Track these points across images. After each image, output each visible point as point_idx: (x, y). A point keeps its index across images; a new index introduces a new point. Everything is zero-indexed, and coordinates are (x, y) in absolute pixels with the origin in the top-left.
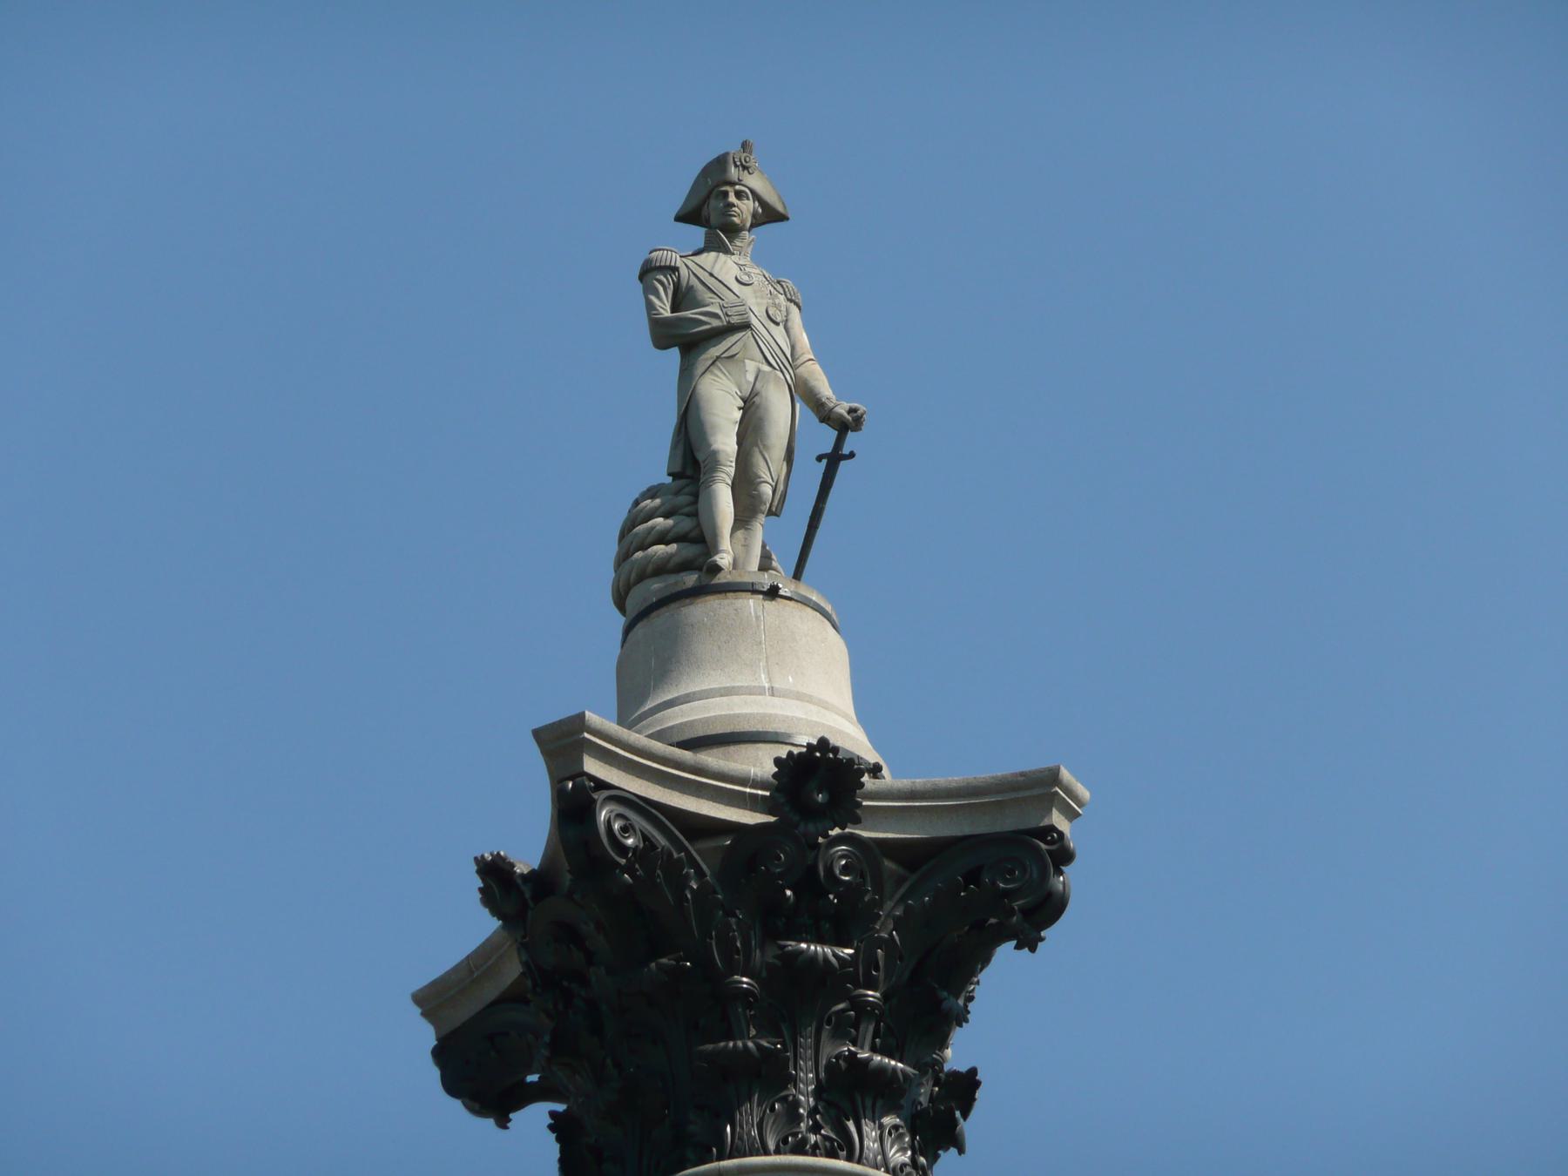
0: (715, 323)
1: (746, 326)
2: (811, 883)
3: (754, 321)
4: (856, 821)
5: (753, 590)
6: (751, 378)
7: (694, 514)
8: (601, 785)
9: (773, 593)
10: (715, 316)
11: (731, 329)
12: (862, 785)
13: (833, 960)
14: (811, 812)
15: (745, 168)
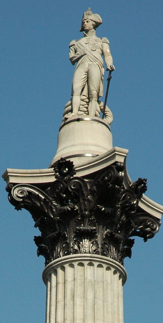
1: (86, 54)
2: (66, 191)
3: (87, 53)
4: (75, 174)
6: (87, 66)
8: (14, 184)
9: (78, 120)
10: (78, 54)
11: (82, 56)
12: (74, 166)
13: (90, 230)
14: (65, 175)
15: (88, 15)
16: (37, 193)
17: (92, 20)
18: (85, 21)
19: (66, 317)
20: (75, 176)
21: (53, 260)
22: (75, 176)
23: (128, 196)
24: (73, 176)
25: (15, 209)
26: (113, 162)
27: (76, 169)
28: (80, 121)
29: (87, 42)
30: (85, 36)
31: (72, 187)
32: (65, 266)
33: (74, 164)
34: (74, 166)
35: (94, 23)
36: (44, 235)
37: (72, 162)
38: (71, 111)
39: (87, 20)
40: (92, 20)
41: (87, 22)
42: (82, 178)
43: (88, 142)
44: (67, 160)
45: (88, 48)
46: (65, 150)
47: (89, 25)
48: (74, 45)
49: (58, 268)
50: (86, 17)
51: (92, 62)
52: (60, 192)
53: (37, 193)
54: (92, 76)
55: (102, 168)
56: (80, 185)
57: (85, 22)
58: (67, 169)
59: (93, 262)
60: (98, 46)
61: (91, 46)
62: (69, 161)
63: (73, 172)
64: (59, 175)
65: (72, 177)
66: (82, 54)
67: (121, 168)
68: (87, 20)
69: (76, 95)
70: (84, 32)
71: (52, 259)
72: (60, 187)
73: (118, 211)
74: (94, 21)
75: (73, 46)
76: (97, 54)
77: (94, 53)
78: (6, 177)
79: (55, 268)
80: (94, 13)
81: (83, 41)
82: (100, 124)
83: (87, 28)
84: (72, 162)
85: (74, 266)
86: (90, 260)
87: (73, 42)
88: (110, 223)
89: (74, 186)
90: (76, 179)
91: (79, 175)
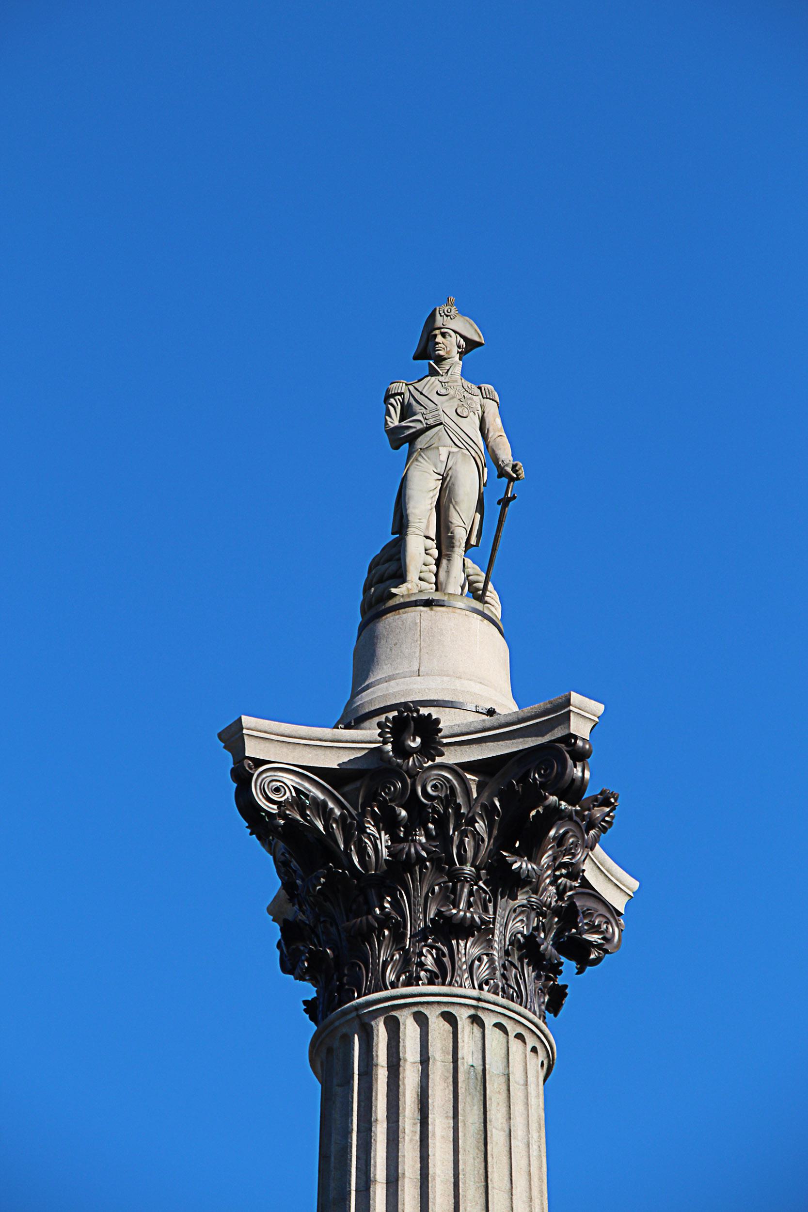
0: (419, 426)
2: (412, 803)
3: (446, 420)
5: (416, 604)
6: (444, 458)
7: (399, 559)
9: (429, 603)
11: (429, 428)
12: (440, 730)
16: (321, 796)
17: (455, 332)
18: (437, 332)
19: (404, 1170)
20: (438, 760)
21: (358, 997)
22: (438, 760)
23: (572, 836)
24: (433, 760)
25: (251, 834)
26: (558, 733)
27: (445, 741)
28: (435, 608)
29: (443, 391)
30: (433, 373)
31: (429, 790)
32: (399, 1017)
33: (440, 726)
34: (440, 730)
35: (462, 342)
36: (322, 919)
37: (437, 721)
38: (401, 577)
39: (442, 330)
40: (455, 332)
41: (444, 335)
42: (460, 770)
43: (461, 666)
44: (424, 711)
45: (447, 408)
46: (392, 683)
47: (449, 346)
48: (401, 394)
49: (376, 1018)
50: (439, 321)
51: (458, 449)
52: (391, 800)
53: (321, 796)
54: (456, 487)
55: (521, 748)
56: (452, 788)
57: (435, 336)
58: (418, 740)
59: (394, 1013)
60: (474, 405)
61: (456, 403)
62: (430, 715)
63: (436, 749)
64: (391, 753)
65: (430, 763)
66: (431, 422)
67: (580, 756)
68: (442, 330)
69: (414, 533)
70: (431, 362)
71: (356, 995)
72: (395, 787)
73: (545, 875)
74: (461, 336)
75: (397, 397)
76: (471, 426)
77: (464, 424)
78: (233, 738)
79: (366, 1020)
80: (462, 312)
81: (431, 385)
82: (486, 621)
83: (441, 353)
84: (437, 721)
85: (427, 1019)
86: (476, 1008)
87: (400, 387)
88: (523, 906)
89: (435, 787)
90: (442, 770)
91: (452, 757)
